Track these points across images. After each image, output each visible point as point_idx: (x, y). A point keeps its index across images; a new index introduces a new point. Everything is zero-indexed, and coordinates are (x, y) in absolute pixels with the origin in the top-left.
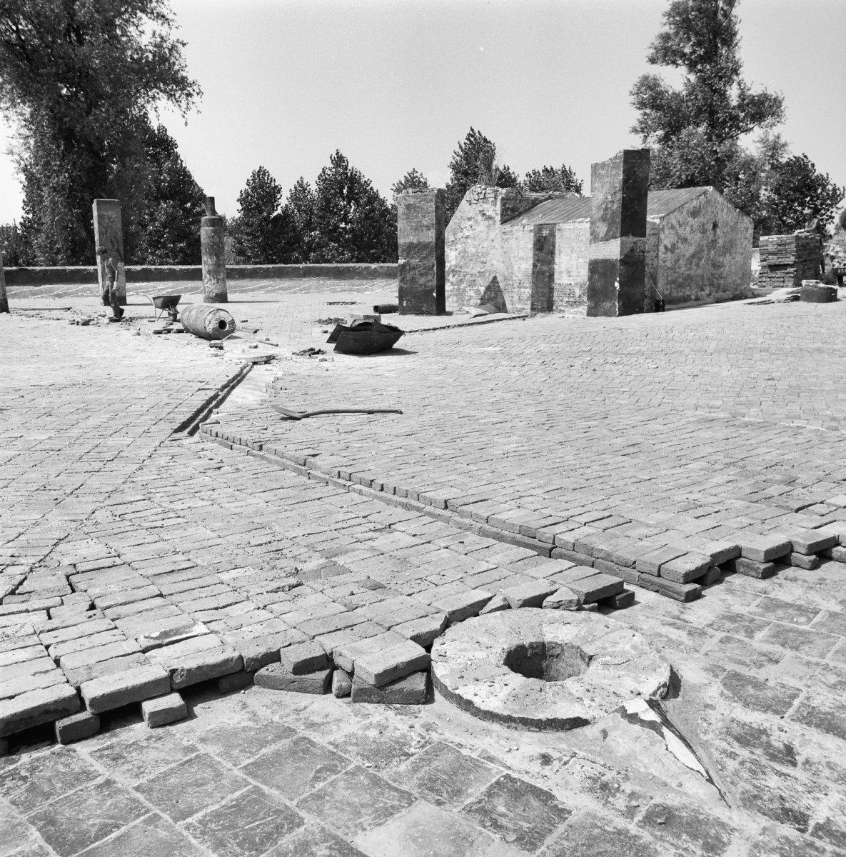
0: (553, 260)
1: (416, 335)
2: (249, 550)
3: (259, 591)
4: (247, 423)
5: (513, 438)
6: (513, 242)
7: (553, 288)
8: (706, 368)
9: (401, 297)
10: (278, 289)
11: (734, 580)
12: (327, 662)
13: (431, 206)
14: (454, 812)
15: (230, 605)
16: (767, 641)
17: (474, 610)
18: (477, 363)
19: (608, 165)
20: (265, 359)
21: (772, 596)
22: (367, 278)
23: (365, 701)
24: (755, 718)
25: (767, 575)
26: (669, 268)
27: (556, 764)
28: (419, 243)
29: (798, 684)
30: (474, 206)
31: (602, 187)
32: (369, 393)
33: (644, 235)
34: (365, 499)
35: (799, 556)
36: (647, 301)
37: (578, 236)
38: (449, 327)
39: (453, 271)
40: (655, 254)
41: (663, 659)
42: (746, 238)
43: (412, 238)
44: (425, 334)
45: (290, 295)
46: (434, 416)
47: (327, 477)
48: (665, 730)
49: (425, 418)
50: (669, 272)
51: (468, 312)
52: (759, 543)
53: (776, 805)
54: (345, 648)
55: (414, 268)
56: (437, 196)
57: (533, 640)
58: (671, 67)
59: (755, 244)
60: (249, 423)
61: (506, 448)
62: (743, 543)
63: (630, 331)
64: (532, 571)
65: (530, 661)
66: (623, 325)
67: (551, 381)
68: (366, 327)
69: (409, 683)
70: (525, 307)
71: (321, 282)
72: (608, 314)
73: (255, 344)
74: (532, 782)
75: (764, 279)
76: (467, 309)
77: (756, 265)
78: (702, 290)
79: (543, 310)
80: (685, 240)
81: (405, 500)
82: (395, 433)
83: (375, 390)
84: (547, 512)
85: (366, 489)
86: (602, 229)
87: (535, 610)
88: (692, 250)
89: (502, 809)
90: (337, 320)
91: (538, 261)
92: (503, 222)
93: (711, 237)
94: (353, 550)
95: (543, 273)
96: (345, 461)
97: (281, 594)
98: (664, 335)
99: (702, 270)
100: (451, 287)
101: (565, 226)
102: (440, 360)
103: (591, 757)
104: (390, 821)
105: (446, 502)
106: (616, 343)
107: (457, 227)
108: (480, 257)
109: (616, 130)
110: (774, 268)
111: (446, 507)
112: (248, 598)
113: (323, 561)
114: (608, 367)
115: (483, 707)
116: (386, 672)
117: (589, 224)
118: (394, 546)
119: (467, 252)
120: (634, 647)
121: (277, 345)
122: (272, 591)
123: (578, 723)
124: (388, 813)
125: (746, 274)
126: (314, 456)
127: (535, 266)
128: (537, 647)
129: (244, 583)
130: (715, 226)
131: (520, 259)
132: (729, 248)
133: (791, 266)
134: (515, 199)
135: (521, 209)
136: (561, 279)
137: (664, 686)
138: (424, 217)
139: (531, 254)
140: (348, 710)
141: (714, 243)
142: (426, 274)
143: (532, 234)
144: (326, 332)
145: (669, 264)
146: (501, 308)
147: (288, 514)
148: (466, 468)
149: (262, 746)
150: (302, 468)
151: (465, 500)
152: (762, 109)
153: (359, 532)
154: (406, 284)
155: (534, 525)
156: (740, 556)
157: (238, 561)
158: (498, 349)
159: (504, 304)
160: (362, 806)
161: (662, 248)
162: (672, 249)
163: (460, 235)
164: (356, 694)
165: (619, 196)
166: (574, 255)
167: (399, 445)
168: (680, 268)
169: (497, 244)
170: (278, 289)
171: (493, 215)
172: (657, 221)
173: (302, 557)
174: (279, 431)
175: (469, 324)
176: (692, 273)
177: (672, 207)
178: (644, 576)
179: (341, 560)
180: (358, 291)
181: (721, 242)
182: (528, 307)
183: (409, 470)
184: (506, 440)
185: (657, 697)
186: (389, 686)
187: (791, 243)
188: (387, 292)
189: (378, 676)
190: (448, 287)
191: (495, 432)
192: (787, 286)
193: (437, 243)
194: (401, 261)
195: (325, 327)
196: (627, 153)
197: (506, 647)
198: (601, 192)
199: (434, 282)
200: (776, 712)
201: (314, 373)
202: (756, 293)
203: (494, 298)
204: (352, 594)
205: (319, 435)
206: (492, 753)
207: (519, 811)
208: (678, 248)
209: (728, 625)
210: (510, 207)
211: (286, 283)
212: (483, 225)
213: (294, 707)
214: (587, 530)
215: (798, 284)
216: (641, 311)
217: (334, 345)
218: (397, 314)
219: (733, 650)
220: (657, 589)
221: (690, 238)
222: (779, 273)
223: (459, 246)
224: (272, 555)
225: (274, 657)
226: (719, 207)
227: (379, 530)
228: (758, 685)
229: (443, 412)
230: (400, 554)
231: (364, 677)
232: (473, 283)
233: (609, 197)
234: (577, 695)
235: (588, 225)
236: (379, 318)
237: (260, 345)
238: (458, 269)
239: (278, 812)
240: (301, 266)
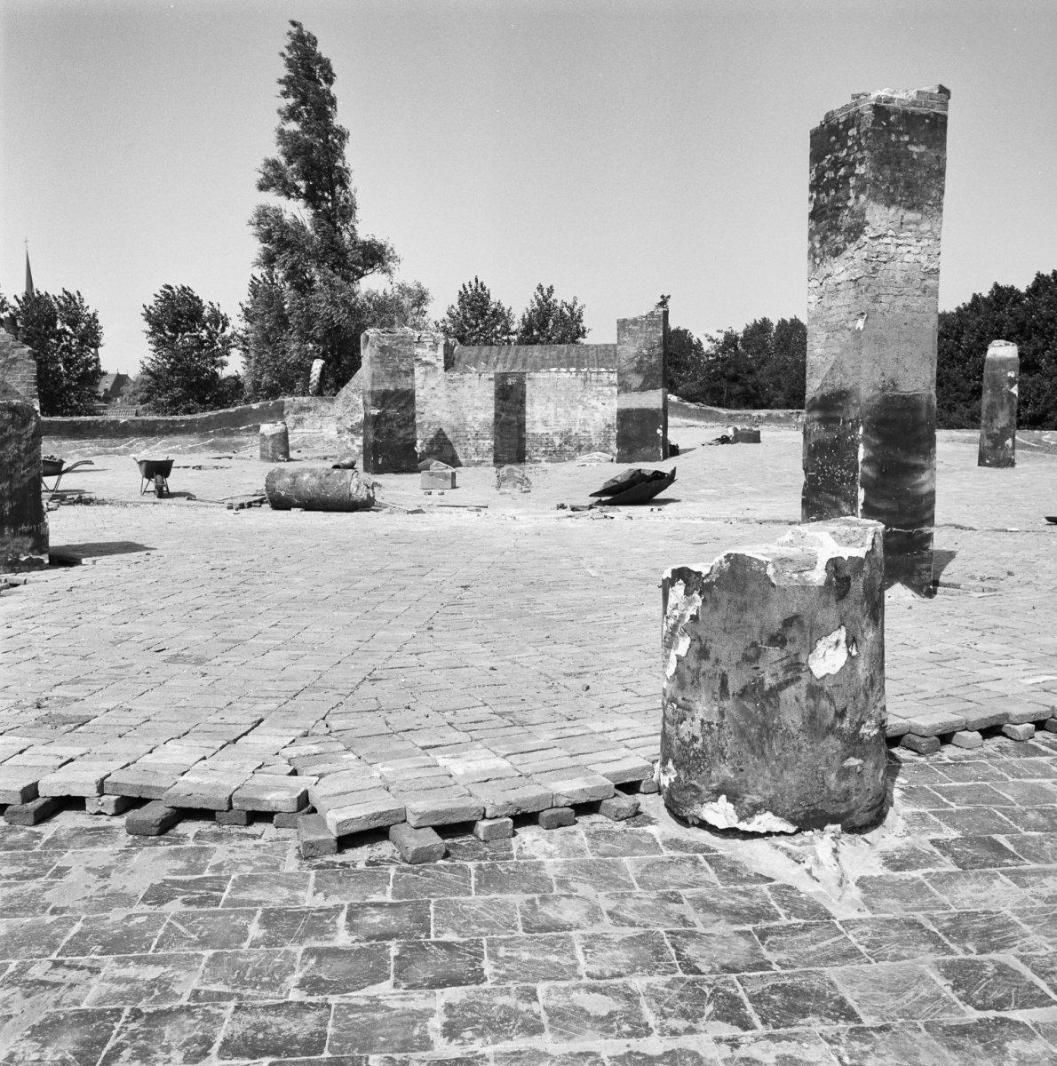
6: (465, 391)
22: (115, 437)
28: (397, 391)
31: (635, 342)
70: (485, 459)
91: (502, 410)
95: (510, 423)
101: (541, 376)
117: (616, 375)
127: (497, 415)
138: (401, 361)
139: (492, 403)
143: (493, 383)
152: (374, 256)
154: (381, 438)
166: (551, 405)
171: (433, 360)
233: (645, 351)
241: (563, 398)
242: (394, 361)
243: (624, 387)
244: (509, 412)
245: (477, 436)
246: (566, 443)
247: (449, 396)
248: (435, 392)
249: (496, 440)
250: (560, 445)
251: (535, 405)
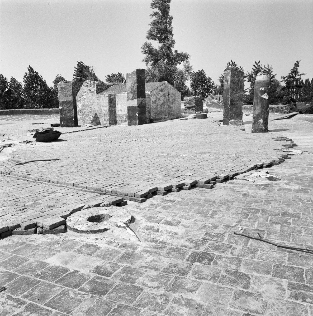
0: (116, 106)
1: (67, 134)
2: (8, 202)
3: (12, 211)
4: (3, 166)
5: (98, 165)
6: (101, 100)
8: (164, 141)
9: (61, 121)
10: (12, 119)
11: (156, 197)
12: (35, 225)
13: (70, 88)
14: (71, 252)
15: (3, 216)
16: (160, 209)
17: (80, 209)
18: (88, 143)
19: (132, 74)
20: (8, 145)
21: (165, 199)
22: (48, 114)
23: (47, 234)
24: (152, 225)
25: (164, 194)
26: (154, 109)
27: (99, 240)
29: (164, 216)
30: (86, 88)
31: (130, 82)
32: (49, 155)
33: (145, 98)
34: (47, 185)
35: (174, 189)
36: (148, 120)
37: (123, 98)
38: (79, 131)
39: (80, 111)
40: (149, 104)
41: (130, 214)
42: (179, 98)
43: (64, 99)
44: (70, 134)
45: (17, 121)
46: (71, 160)
47: (34, 181)
48: (127, 228)
49: (68, 161)
50: (154, 110)
51: (86, 126)
52: (162, 186)
53: (152, 239)
54: (40, 222)
55: (65, 110)
56: (72, 84)
57: (96, 214)
58: (154, 41)
59: (182, 100)
60: (4, 166)
61: (95, 168)
62: (158, 187)
63: (142, 130)
64: (98, 198)
65: (96, 219)
66: (139, 128)
67: (113, 147)
68: (47, 132)
69: (60, 227)
70: (107, 123)
71: (30, 116)
72: (135, 124)
73: (4, 140)
74: (93, 244)
75: (186, 112)
76: (86, 124)
77: (183, 107)
78: (166, 115)
79: (113, 124)
80: (159, 99)
81: (61, 185)
82: (58, 166)
83: (51, 153)
84: (105, 184)
85: (48, 183)
86: (131, 96)
87: (97, 207)
88: (161, 102)
89: (84, 250)
90: (36, 130)
91: (110, 107)
92: (97, 93)
93: (168, 98)
94: (43, 199)
95: (112, 111)
96: (40, 175)
97: (20, 212)
98: (153, 131)
99: (165, 109)
100: (80, 117)
101: (119, 95)
102: (75, 142)
103: (108, 237)
104: (54, 256)
105: (73, 184)
106: (137, 134)
107: (81, 95)
108: (90, 106)
109: (136, 61)
110: (189, 108)
111: (74, 186)
112: (9, 213)
113: (33, 202)
114: (133, 142)
115: (80, 230)
116: (52, 225)
118: (56, 196)
119: (85, 104)
120: (123, 213)
121: (13, 140)
122: (16, 211)
123: (105, 230)
124: (53, 255)
125: (180, 110)
126: (29, 175)
127: (109, 108)
128: (97, 216)
129: (7, 210)
130: (169, 94)
131: (104, 106)
132: (174, 102)
133: (194, 107)
134: (101, 85)
136: (119, 113)
137: (129, 220)
138: (68, 91)
140: (42, 236)
141: (168, 100)
142: (70, 112)
143: (108, 98)
144: (32, 134)
145: (154, 107)
146: (99, 123)
147: (20, 191)
148: (81, 174)
149: (16, 247)
150: (25, 179)
151: (80, 183)
153: (45, 194)
155: (100, 187)
156: (158, 190)
157: (4, 205)
158: (96, 138)
159: (100, 122)
160: (46, 254)
161: (151, 102)
162: (155, 102)
163: (82, 98)
164: (44, 232)
165: (136, 84)
166: (123, 105)
167: (59, 169)
168: (158, 108)
169: (96, 101)
170: (12, 119)
171: (94, 91)
172: (149, 93)
173: (26, 202)
174: (16, 168)
175: (87, 130)
176: (162, 110)
177: (154, 88)
178: (130, 197)
179: (39, 202)
180: (45, 119)
181: (171, 100)
183: (62, 176)
184: (95, 166)
185: (127, 223)
186: (54, 229)
187: (193, 100)
188: (56, 119)
189: (50, 226)
190: (79, 117)
191: (92, 164)
192: (193, 114)
193: (73, 101)
194: (60, 108)
195: (32, 133)
196: (137, 70)
197: (88, 217)
198: (131, 83)
199: (73, 115)
200: (157, 223)
201: (28, 149)
202: (184, 116)
203: (96, 121)
204: (43, 209)
205: (30, 169)
206: (82, 240)
207: (88, 249)
208: (157, 102)
209: (151, 206)
211: (15, 117)
212: (90, 94)
213: (25, 238)
214: (116, 187)
215: (196, 113)
216: (146, 123)
217: (35, 139)
218: (60, 127)
219: (151, 212)
220: (134, 200)
221: (160, 98)
222: (190, 110)
223: (82, 102)
224: (16, 202)
225: (19, 226)
226: (169, 88)
227: (52, 193)
228: (154, 218)
229: (75, 159)
230: (58, 198)
231: (46, 227)
232: (88, 115)
234: (106, 224)
235: (126, 94)
236: (53, 129)
237: (6, 140)
238: (82, 110)
239: (22, 259)
240: (21, 110)
242: (65, 92)
243: (129, 99)
245: (105, 115)
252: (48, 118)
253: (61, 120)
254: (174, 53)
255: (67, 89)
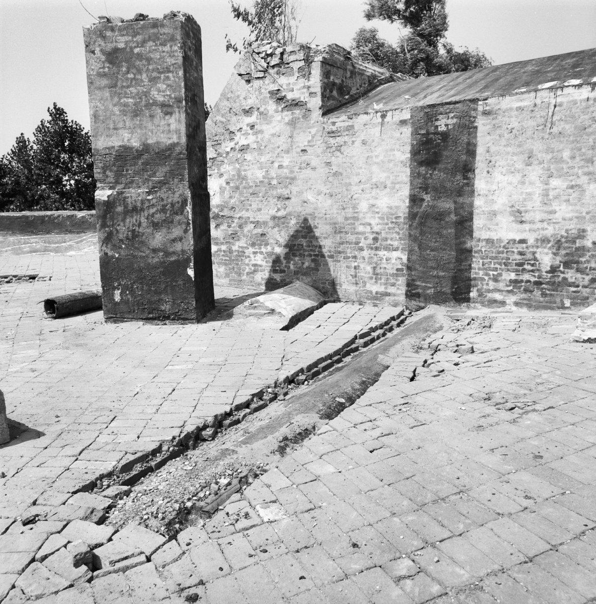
0: (470, 184)
6: (355, 151)
7: (470, 251)
22: (71, 232)
28: (146, 148)
30: (256, 84)
43: (126, 135)
51: (272, 311)
55: (135, 210)
58: (387, 22)
70: (391, 290)
91: (425, 188)
92: (327, 111)
95: (440, 216)
119: (244, 178)
127: (415, 200)
135: (353, 91)
138: (154, 80)
139: (405, 174)
142: (168, 223)
143: (407, 131)
154: (115, 248)
163: (227, 146)
166: (535, 173)
171: (303, 96)
180: (57, 251)
182: (399, 290)
193: (190, 148)
199: (189, 243)
210: (338, 81)
212: (278, 121)
238: (226, 212)
241: (566, 154)
244: (440, 191)
246: (567, 265)
247: (328, 164)
248: (305, 158)
249: (411, 252)
250: (553, 270)
251: (497, 176)
252: (70, 248)
253: (109, 270)
254: (442, 51)
255: (149, 60)
